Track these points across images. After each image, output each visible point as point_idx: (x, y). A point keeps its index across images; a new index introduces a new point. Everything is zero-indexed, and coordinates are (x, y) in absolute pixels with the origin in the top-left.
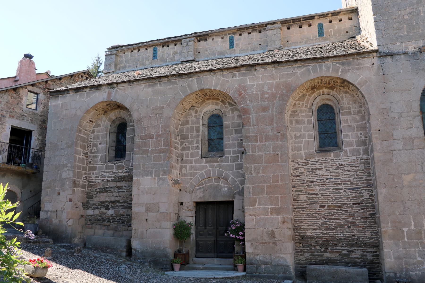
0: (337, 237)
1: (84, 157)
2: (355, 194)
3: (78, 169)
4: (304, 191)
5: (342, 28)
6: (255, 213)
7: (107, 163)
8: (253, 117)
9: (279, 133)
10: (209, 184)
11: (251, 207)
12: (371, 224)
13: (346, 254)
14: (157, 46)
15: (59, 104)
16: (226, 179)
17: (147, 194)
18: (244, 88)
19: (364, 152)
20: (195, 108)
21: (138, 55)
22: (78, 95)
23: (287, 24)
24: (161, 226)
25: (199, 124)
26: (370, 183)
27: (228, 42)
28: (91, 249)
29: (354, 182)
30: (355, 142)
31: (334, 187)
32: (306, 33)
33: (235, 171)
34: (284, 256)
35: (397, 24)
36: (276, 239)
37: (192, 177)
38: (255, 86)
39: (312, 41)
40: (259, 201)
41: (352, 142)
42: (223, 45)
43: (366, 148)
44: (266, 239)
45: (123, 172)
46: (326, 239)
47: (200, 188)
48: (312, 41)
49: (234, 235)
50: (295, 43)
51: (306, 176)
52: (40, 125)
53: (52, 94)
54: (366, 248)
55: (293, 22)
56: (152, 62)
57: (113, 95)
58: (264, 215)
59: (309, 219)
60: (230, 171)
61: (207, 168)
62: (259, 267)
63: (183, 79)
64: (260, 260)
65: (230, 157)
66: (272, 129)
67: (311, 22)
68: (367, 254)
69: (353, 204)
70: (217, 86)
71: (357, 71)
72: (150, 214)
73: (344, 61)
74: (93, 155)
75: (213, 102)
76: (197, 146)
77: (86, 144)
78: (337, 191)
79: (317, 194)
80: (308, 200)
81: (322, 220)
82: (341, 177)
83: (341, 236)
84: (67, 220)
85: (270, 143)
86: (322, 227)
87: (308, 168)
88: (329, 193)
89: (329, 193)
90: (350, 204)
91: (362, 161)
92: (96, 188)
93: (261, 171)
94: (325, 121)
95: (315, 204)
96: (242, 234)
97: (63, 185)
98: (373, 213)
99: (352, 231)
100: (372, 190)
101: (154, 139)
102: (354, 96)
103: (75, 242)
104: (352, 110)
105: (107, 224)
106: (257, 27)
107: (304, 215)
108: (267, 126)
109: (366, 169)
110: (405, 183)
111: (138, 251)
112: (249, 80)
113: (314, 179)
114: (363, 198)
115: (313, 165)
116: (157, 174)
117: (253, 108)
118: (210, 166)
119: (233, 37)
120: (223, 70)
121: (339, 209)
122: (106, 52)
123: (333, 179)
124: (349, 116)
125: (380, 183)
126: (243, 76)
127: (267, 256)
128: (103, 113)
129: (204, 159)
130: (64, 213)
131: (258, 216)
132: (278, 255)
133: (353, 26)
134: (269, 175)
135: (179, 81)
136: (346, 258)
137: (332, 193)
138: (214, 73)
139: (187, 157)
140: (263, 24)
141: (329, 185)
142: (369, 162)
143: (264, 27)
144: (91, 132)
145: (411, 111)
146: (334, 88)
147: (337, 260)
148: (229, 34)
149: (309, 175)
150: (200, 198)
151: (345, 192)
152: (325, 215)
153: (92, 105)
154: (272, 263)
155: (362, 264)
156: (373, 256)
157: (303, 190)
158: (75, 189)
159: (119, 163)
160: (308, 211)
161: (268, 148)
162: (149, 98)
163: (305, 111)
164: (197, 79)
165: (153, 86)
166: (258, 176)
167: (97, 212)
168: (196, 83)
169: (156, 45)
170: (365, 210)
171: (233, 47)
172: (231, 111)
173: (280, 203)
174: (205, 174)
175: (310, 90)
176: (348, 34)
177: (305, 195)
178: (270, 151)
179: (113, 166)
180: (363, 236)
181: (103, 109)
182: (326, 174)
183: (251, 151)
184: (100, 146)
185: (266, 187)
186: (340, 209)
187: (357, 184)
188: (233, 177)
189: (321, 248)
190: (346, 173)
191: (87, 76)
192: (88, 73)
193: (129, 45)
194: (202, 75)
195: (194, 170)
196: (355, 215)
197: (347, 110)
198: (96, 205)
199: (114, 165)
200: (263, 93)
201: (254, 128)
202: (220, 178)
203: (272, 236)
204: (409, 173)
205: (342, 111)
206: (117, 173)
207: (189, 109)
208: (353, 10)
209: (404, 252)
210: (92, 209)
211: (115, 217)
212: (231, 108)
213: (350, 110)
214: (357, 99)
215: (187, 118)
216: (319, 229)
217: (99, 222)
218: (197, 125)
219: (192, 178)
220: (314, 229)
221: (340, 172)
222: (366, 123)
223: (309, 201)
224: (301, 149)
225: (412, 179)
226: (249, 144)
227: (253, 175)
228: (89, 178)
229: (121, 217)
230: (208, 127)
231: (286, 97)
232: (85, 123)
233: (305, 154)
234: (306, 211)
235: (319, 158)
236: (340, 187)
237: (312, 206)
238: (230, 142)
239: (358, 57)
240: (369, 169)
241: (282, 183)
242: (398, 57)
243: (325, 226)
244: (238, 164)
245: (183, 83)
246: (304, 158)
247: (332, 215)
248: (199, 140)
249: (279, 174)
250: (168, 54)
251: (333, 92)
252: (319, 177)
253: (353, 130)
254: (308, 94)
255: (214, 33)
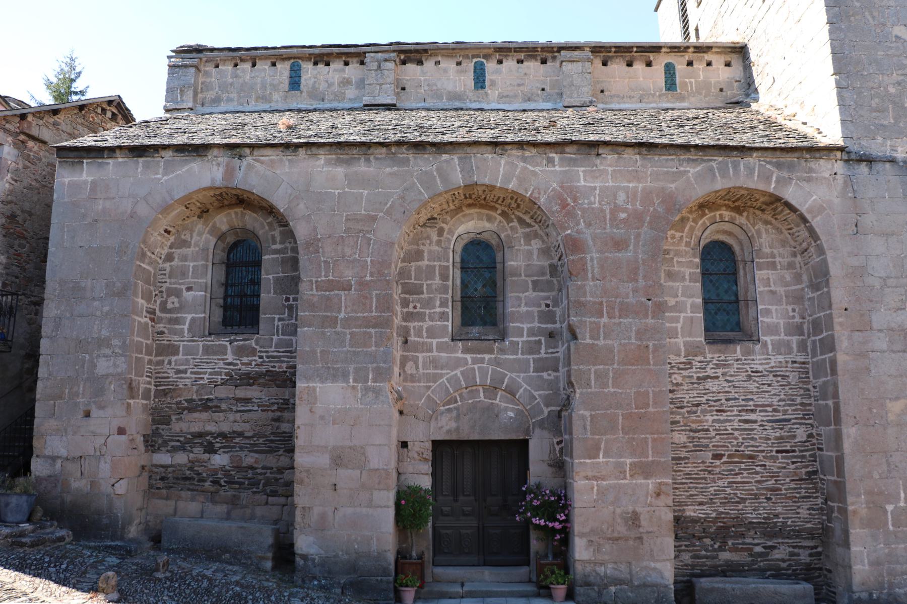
0: (745, 518)
1: (147, 320)
2: (780, 431)
3: (137, 352)
4: (682, 424)
5: (713, 81)
6: (597, 474)
7: (209, 339)
8: (592, 259)
9: (649, 300)
10: (470, 401)
11: (588, 461)
12: (810, 493)
13: (762, 553)
14: (300, 61)
15: (85, 182)
16: (511, 392)
17: (333, 424)
18: (571, 192)
19: (799, 347)
20: (436, 223)
21: (253, 75)
22: (141, 165)
23: (602, 55)
24: (371, 500)
25: (448, 261)
26: (809, 410)
27: (471, 75)
28: (179, 553)
29: (779, 408)
30: (782, 327)
31: (741, 416)
32: (641, 79)
33: (531, 374)
34: (658, 565)
35: (877, 100)
36: (641, 530)
37: (431, 384)
38: (597, 192)
39: (653, 97)
40: (605, 447)
41: (776, 326)
42: (460, 80)
43: (802, 339)
44: (622, 529)
45: (254, 363)
46: (724, 523)
47: (449, 410)
48: (653, 97)
49: (543, 521)
50: (618, 96)
51: (685, 392)
52: (3, 225)
53: (64, 153)
54: (798, 540)
55: (615, 52)
56: (286, 97)
57: (240, 175)
58: (616, 478)
59: (691, 483)
60: (522, 375)
61: (467, 364)
62: (605, 591)
63: (426, 156)
64: (606, 575)
65: (520, 343)
66: (635, 291)
67: (652, 58)
68: (801, 551)
69: (778, 452)
70: (509, 182)
71: (804, 184)
72: (342, 472)
73: (782, 160)
74: (168, 315)
75: (479, 214)
76: (443, 313)
77: (152, 288)
78: (747, 426)
79: (708, 430)
80: (690, 442)
81: (717, 484)
82: (754, 397)
83: (752, 517)
84: (114, 481)
85: (631, 320)
86: (716, 499)
87: (691, 374)
88: (732, 429)
89: (732, 429)
90: (771, 451)
91: (795, 365)
92: (179, 399)
93: (610, 381)
94: (716, 277)
95: (704, 451)
96: (564, 518)
97: (99, 392)
98: (814, 471)
99: (773, 506)
100: (812, 426)
101: (353, 292)
102: (782, 233)
103: (131, 536)
104: (778, 259)
105: (212, 489)
106: (538, 51)
107: (682, 473)
108: (623, 282)
109: (802, 382)
110: (891, 417)
111: (314, 560)
112: (584, 177)
113: (701, 399)
114: (796, 441)
115: (700, 368)
116: (361, 377)
117: (593, 240)
118: (475, 361)
119: (482, 64)
120: (524, 146)
121: (749, 462)
122: (169, 57)
123: (738, 399)
124: (773, 272)
125: (847, 415)
126: (569, 165)
127: (623, 567)
128: (198, 212)
129: (460, 344)
130: (102, 462)
131: (603, 479)
132: (645, 563)
133: (733, 81)
134: (628, 391)
135: (415, 158)
136: (761, 561)
137: (737, 429)
138: (502, 150)
139: (419, 337)
140: (553, 46)
141: (732, 411)
142: (808, 368)
143: (554, 52)
144: (163, 257)
145: (902, 276)
146: (744, 211)
147: (743, 565)
148: (474, 56)
149: (691, 390)
150: (449, 431)
151: (762, 428)
152: (723, 475)
153: (181, 195)
154: (632, 583)
155: (790, 572)
156: (811, 555)
157: (679, 422)
158: (132, 401)
159: (241, 340)
160: (689, 465)
161: (627, 331)
162: (337, 192)
163: (686, 252)
164: (460, 158)
165: (348, 162)
166: (604, 392)
167: (181, 458)
168: (459, 169)
169: (299, 58)
170: (799, 464)
171: (483, 87)
172: (524, 237)
173: (650, 452)
174: (461, 378)
175: (696, 211)
176: (724, 93)
177: (684, 433)
178: (630, 338)
179: (225, 346)
180: (794, 516)
181: (201, 204)
182: (727, 389)
183: (588, 337)
184: (188, 295)
185: (621, 418)
186: (752, 462)
187: (785, 412)
188: (529, 388)
189: (712, 542)
190: (766, 388)
191: (115, 111)
192: (119, 103)
193: (230, 49)
194: (475, 152)
195: (436, 368)
196: (780, 474)
197: (767, 258)
198: (178, 441)
199: (228, 344)
200: (616, 209)
201: (596, 286)
202: (496, 388)
203: (633, 523)
204: (897, 398)
205: (758, 260)
206: (236, 365)
207: (424, 225)
208: (735, 48)
209: (887, 551)
210: (168, 451)
211: (233, 473)
212: (523, 230)
213: (773, 260)
214: (787, 238)
215: (418, 245)
216: (711, 501)
217: (188, 482)
218: (442, 264)
219: (429, 387)
220: (701, 504)
221: (752, 386)
222: (803, 289)
223: (691, 445)
224: (677, 334)
225: (902, 410)
226: (584, 319)
227: (593, 390)
228: (159, 373)
229: (247, 471)
230: (462, 268)
231: (664, 223)
232: (155, 237)
233: (684, 346)
234: (686, 465)
235: (712, 355)
236: (753, 417)
237: (697, 455)
238: (522, 308)
239: (808, 156)
240: (808, 383)
241: (656, 410)
242: (878, 167)
243: (722, 496)
244: (541, 359)
245: (426, 164)
246: (683, 354)
247: (736, 474)
248: (447, 299)
249: (650, 390)
250: (327, 81)
251: (742, 220)
252: (711, 395)
253: (779, 302)
254: (691, 216)
255: (442, 49)
